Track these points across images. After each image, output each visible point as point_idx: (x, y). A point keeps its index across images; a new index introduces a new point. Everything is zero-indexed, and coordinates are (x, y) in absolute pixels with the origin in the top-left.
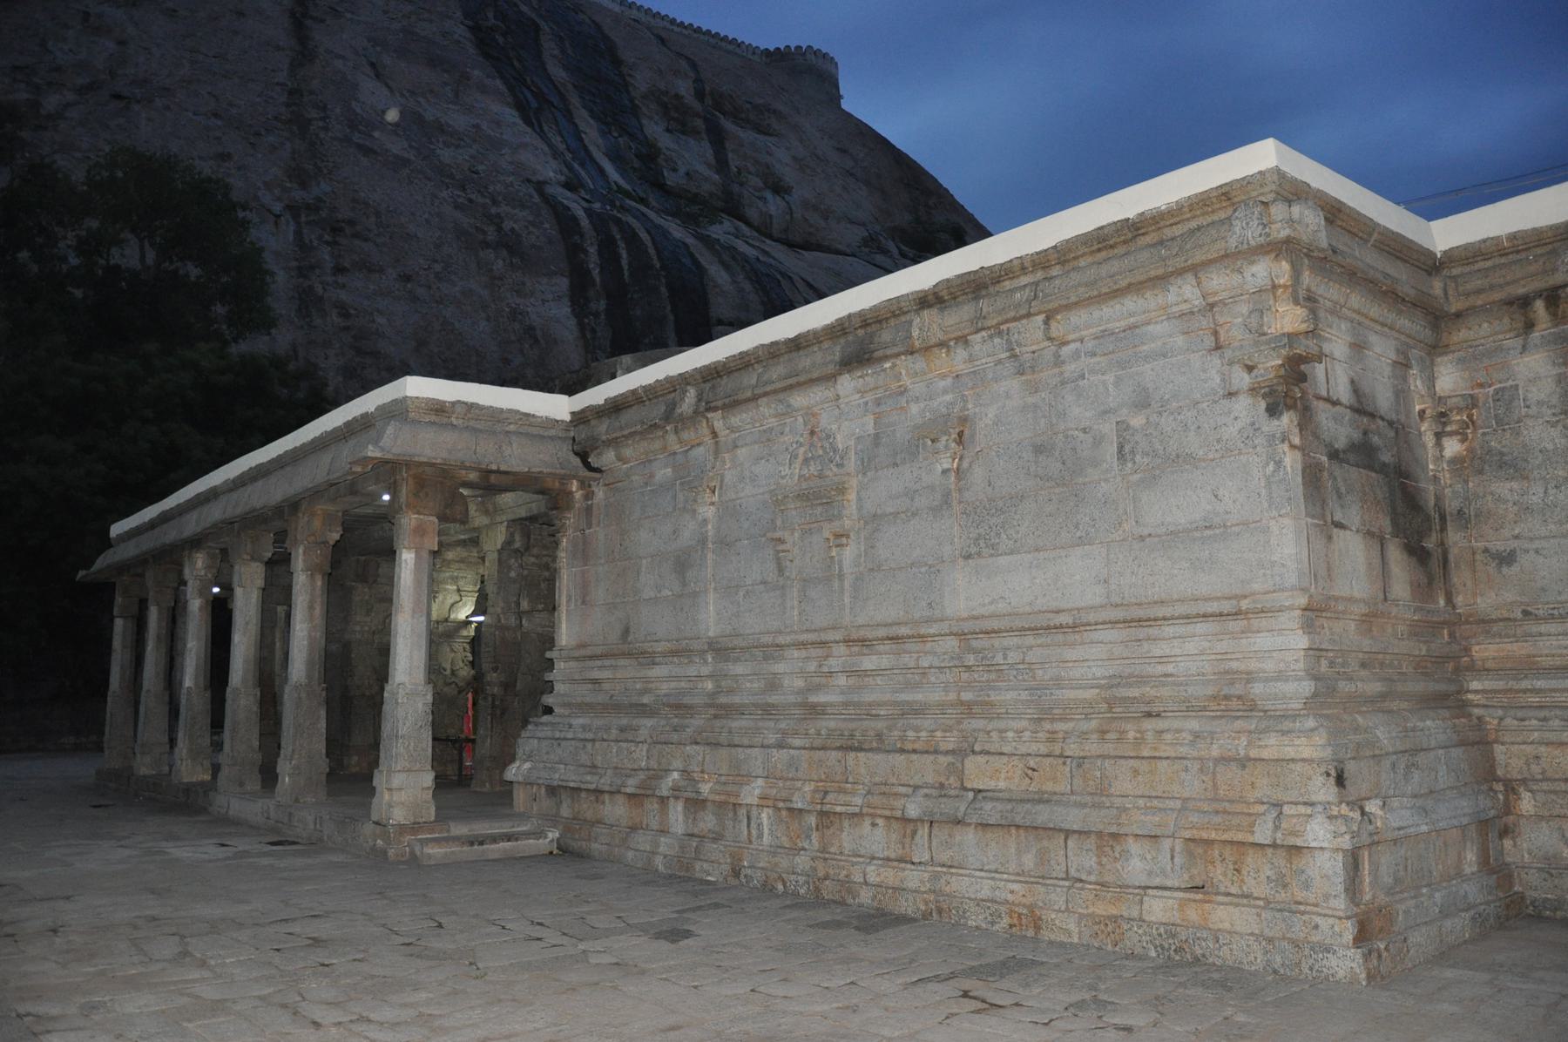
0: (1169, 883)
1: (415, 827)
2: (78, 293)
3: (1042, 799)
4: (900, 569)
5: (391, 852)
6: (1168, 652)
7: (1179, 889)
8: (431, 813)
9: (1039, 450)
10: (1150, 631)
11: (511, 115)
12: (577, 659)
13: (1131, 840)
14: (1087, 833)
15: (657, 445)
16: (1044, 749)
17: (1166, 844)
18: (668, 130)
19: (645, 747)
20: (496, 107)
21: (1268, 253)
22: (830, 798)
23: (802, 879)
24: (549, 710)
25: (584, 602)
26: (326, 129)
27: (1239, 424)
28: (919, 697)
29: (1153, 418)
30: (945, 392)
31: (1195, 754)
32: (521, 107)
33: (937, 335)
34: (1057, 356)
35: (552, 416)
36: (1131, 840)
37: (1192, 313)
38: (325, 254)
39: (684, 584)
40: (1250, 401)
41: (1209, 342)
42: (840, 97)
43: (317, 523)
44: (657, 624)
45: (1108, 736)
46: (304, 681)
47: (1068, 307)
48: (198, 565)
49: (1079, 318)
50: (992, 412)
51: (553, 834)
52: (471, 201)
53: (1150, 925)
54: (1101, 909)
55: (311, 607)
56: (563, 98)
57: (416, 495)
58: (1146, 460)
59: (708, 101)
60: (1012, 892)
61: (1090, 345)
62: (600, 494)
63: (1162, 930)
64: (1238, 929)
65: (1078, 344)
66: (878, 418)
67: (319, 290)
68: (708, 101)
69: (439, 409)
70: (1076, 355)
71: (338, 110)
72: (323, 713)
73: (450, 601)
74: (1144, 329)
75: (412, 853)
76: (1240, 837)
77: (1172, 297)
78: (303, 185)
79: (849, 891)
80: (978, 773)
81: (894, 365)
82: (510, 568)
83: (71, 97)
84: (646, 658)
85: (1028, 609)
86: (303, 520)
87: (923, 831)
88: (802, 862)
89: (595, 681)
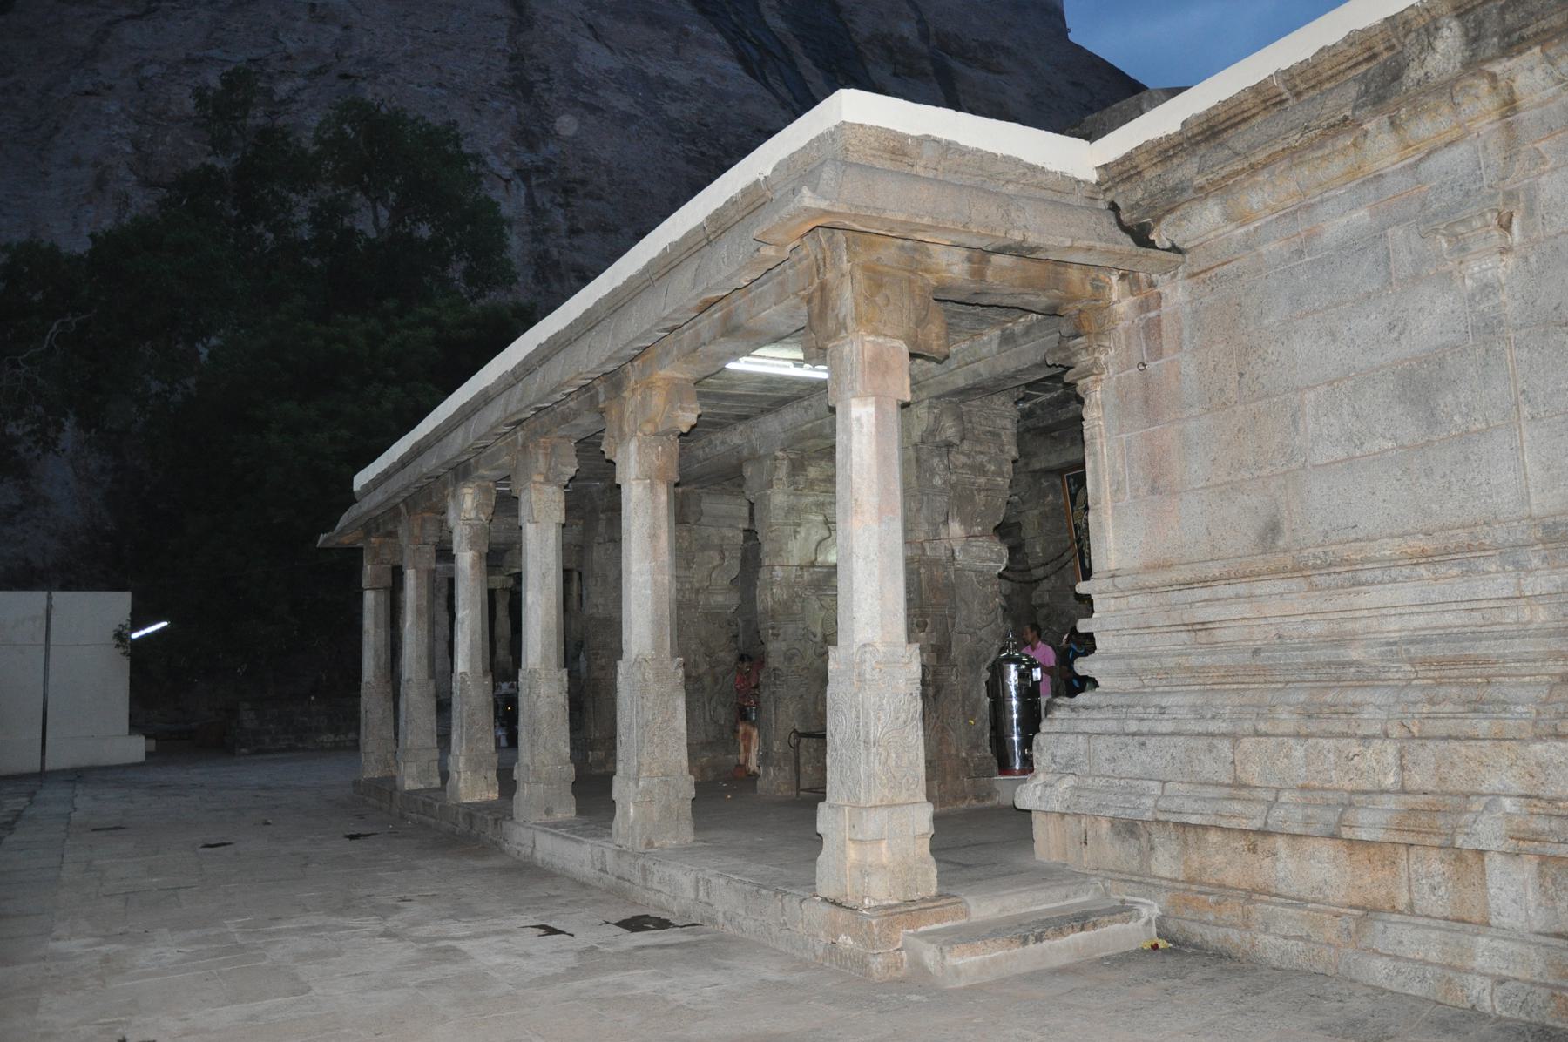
1: (907, 910)
2: (315, 263)
5: (877, 964)
8: (929, 878)
11: (733, 67)
12: (1152, 590)
15: (1337, 167)
18: (895, 74)
19: (1391, 749)
20: (718, 61)
24: (1088, 683)
25: (1153, 490)
26: (550, 90)
32: (743, 60)
35: (1071, 173)
38: (558, 215)
42: (1067, 31)
43: (658, 401)
46: (649, 652)
48: (467, 508)
51: (1150, 909)
52: (702, 154)
55: (653, 537)
56: (784, 48)
57: (870, 300)
59: (933, 42)
62: (1176, 293)
67: (554, 252)
68: (933, 42)
69: (898, 148)
71: (560, 72)
72: (681, 703)
73: (815, 538)
75: (917, 963)
78: (531, 147)
82: (933, 473)
83: (300, 82)
84: (1340, 569)
86: (632, 399)
89: (1204, 626)
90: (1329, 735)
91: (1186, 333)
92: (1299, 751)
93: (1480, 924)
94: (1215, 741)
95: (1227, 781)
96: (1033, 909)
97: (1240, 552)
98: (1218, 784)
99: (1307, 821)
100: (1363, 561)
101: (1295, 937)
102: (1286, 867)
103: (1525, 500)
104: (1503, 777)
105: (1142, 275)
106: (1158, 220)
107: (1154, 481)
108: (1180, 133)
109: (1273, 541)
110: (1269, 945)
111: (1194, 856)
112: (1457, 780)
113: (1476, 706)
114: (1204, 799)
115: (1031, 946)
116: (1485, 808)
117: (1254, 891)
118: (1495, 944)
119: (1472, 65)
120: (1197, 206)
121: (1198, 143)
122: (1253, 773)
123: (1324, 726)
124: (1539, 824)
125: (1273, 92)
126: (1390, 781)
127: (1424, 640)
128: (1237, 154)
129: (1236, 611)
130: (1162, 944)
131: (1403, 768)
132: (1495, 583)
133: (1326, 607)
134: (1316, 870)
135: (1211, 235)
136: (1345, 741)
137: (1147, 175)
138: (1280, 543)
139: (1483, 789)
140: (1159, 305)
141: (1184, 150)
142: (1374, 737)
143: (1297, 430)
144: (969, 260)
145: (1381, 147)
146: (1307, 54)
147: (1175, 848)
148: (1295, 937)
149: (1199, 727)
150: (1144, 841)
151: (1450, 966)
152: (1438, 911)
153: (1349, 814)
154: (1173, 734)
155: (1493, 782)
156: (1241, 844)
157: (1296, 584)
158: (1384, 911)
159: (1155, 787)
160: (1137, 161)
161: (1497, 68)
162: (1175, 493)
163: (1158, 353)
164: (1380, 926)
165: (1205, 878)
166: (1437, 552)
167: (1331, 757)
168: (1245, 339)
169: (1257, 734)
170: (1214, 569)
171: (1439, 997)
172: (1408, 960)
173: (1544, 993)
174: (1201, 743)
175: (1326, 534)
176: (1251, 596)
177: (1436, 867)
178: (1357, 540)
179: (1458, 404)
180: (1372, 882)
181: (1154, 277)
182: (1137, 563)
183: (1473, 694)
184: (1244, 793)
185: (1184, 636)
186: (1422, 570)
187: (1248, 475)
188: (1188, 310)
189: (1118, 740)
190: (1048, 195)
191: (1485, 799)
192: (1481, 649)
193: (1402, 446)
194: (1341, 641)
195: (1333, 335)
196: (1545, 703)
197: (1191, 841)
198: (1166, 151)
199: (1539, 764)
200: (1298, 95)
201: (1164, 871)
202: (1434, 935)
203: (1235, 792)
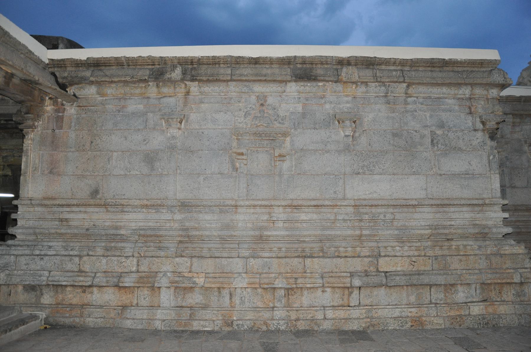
0: (474, 300)
3: (419, 273)
4: (317, 175)
6: (458, 217)
7: (479, 302)
9: (395, 135)
10: (445, 209)
12: (45, 206)
13: (459, 286)
14: (440, 285)
15: (138, 91)
16: (416, 253)
17: (473, 286)
19: (135, 260)
21: (498, 87)
22: (299, 281)
23: (282, 322)
24: (13, 237)
25: (51, 172)
27: (478, 141)
28: (333, 233)
29: (446, 132)
30: (347, 102)
31: (481, 253)
33: (355, 77)
34: (405, 101)
35: (41, 58)
36: (459, 286)
37: (463, 99)
39: (152, 169)
40: (482, 134)
41: (467, 111)
44: (113, 188)
45: (444, 248)
47: (419, 84)
49: (422, 89)
50: (371, 116)
53: (474, 316)
54: (452, 313)
58: (443, 147)
60: (410, 312)
61: (421, 100)
62: (71, 110)
63: (480, 317)
64: (507, 313)
65: (415, 99)
66: (304, 106)
70: (415, 103)
74: (444, 100)
76: (509, 281)
77: (461, 92)
79: (316, 324)
80: (384, 264)
81: (324, 85)
84: (120, 207)
85: (389, 197)
87: (356, 292)
88: (279, 314)
89: (67, 220)
90: (115, 256)
91: (73, 124)
92: (104, 261)
93: (158, 307)
94: (73, 258)
95: (76, 270)
96: (5, 318)
97: (83, 197)
98: (73, 272)
99: (107, 282)
100: (127, 205)
101: (100, 318)
102: (96, 297)
103: (175, 194)
104: (167, 267)
105: (59, 100)
106: (71, 85)
107: (52, 169)
108: (86, 61)
109: (96, 196)
110: (90, 321)
111: (60, 296)
112: (154, 268)
113: (160, 248)
114: (68, 277)
115: (8, 333)
116: (163, 275)
117: (83, 305)
118: (163, 311)
119: (182, 80)
120: (88, 86)
121: (91, 66)
122: (87, 268)
123: (113, 253)
124: (177, 279)
125: (121, 62)
126: (134, 269)
127: (144, 229)
128: (107, 76)
129: (81, 216)
130: (48, 326)
131: (138, 265)
132: (165, 215)
133: (113, 217)
134: (110, 297)
135: (90, 96)
136: (120, 258)
137: (68, 69)
138: (98, 197)
139: (161, 271)
140: (64, 112)
141: (85, 66)
142: (130, 256)
143: (109, 163)
144: (5, 77)
145: (152, 90)
146: (136, 55)
147: (52, 294)
148: (100, 318)
149: (66, 253)
150: (38, 293)
151: (149, 319)
152: (145, 305)
153: (122, 279)
154: (54, 255)
155: (164, 269)
156: (79, 290)
157: (103, 209)
158: (129, 306)
159: (46, 273)
160: (66, 63)
161: (187, 83)
162: (59, 175)
163: (61, 128)
164: (129, 311)
165: (64, 303)
166: (151, 205)
167: (116, 262)
168: (95, 131)
169: (88, 255)
170: (75, 202)
171: (147, 328)
172: (137, 319)
173: (175, 322)
174: (67, 258)
175: (114, 196)
176: (85, 212)
177: (146, 292)
178: (124, 199)
179: (160, 166)
180: (125, 298)
181: (64, 102)
182: (40, 196)
183: (158, 245)
184: (83, 274)
185: (57, 223)
186: (144, 210)
187: (89, 174)
188: (75, 117)
189: (30, 257)
190: (439, 202)
191: (163, 273)
192: (161, 233)
193: (142, 174)
194: (117, 228)
195: (126, 138)
196: (177, 248)
197: (59, 291)
198: (78, 64)
199: (177, 264)
200: (129, 65)
201: (46, 302)
202: (146, 311)
203: (79, 274)
